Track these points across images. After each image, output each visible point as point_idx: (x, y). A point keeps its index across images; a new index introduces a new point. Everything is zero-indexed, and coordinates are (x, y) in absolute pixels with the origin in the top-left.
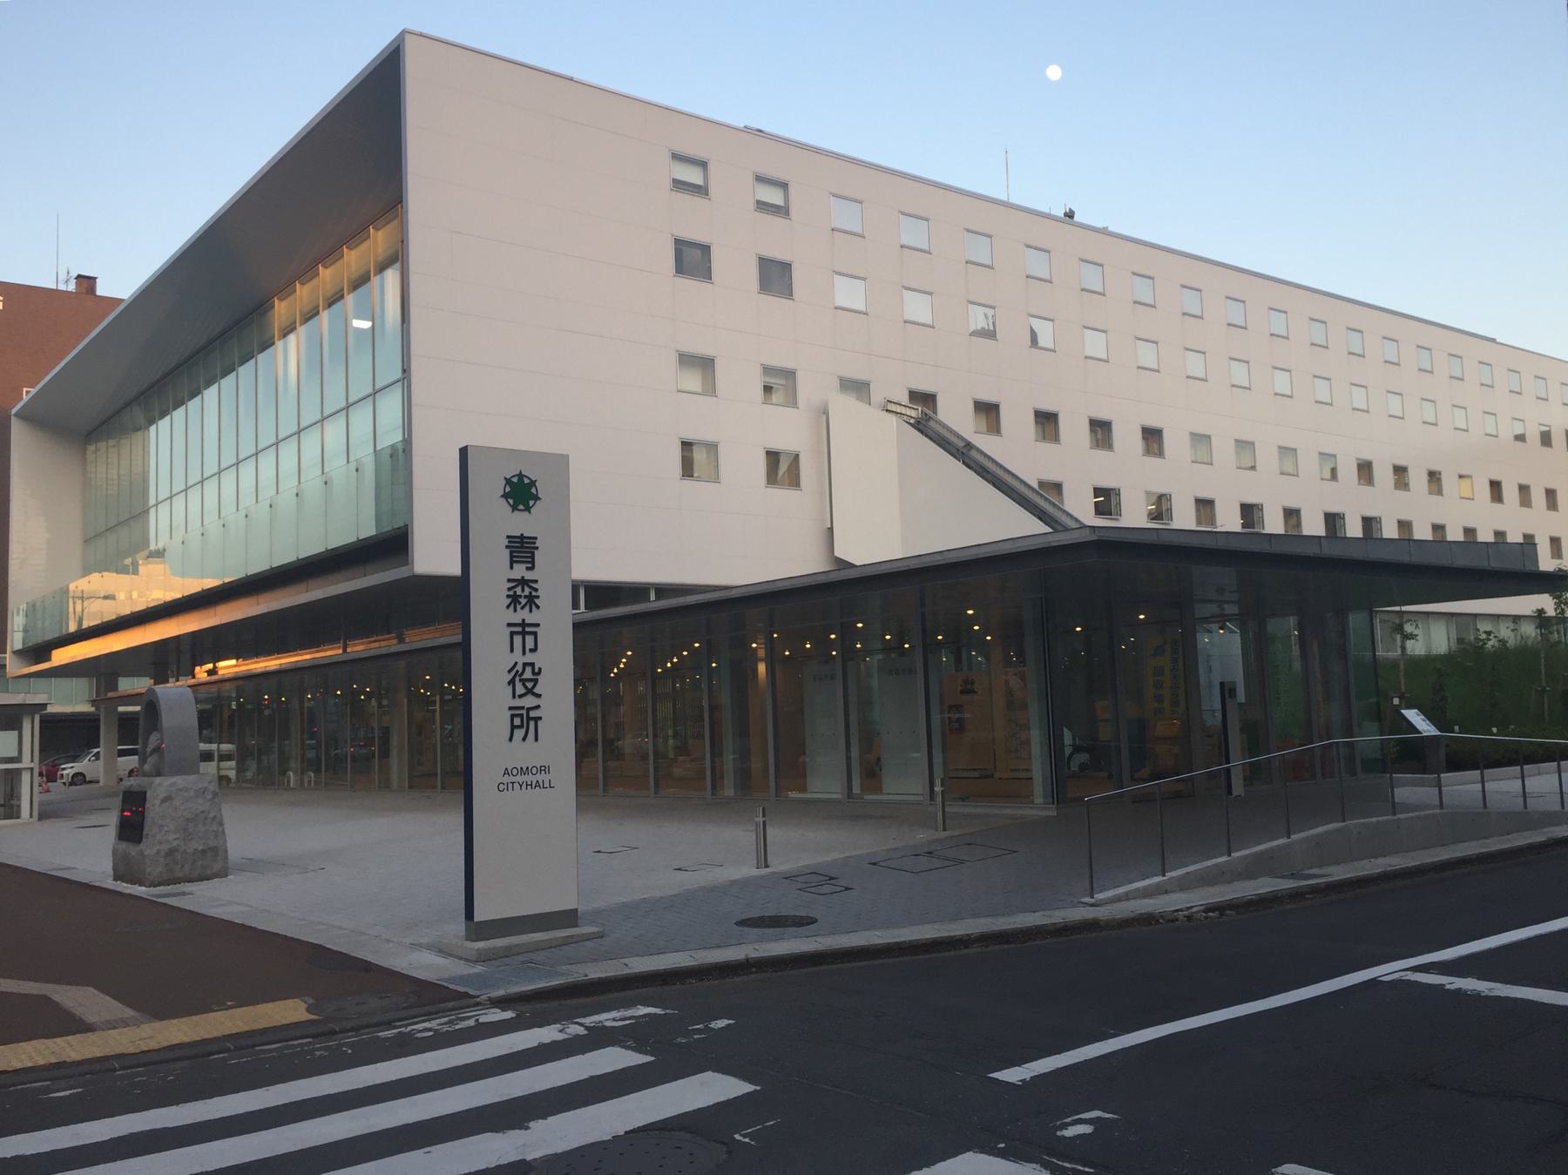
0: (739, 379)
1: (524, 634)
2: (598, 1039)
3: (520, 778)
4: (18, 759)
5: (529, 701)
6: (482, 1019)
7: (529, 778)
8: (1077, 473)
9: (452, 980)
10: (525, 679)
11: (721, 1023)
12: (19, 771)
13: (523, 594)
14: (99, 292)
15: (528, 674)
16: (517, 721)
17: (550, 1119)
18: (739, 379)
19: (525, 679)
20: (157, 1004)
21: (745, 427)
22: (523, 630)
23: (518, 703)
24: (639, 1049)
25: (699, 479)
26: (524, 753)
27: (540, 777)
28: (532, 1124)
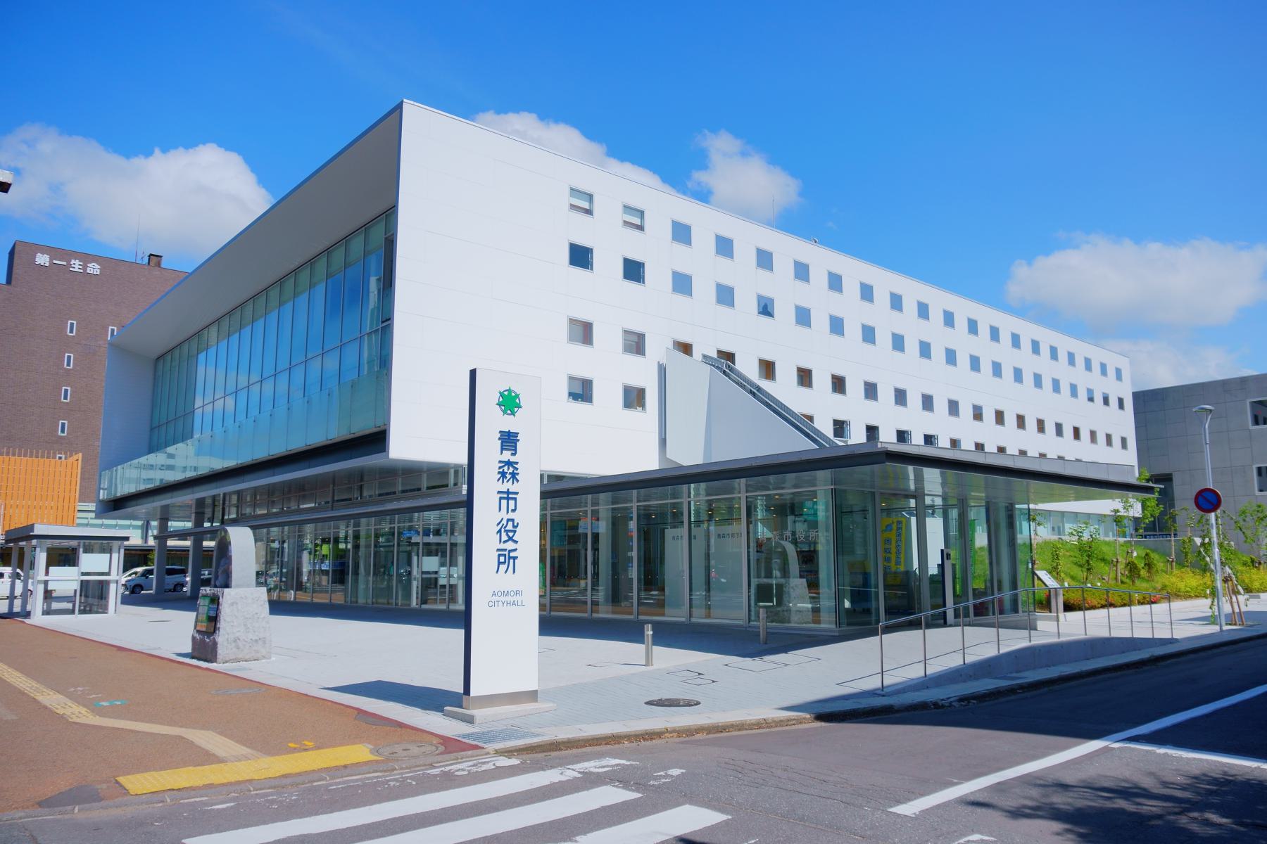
0: (608, 337)
1: (508, 499)
2: (590, 781)
3: (503, 599)
4: (108, 574)
5: (510, 545)
6: (498, 764)
7: (509, 599)
8: (822, 408)
9: (464, 736)
10: (508, 531)
11: (676, 772)
12: (108, 582)
13: (509, 471)
14: (163, 265)
15: (510, 527)
16: (502, 559)
17: (589, 835)
18: (608, 337)
19: (508, 531)
20: (269, 745)
21: (611, 369)
22: (508, 496)
23: (502, 546)
24: (637, 790)
25: (387, 423)
26: (506, 580)
27: (517, 598)
28: (578, 838)
